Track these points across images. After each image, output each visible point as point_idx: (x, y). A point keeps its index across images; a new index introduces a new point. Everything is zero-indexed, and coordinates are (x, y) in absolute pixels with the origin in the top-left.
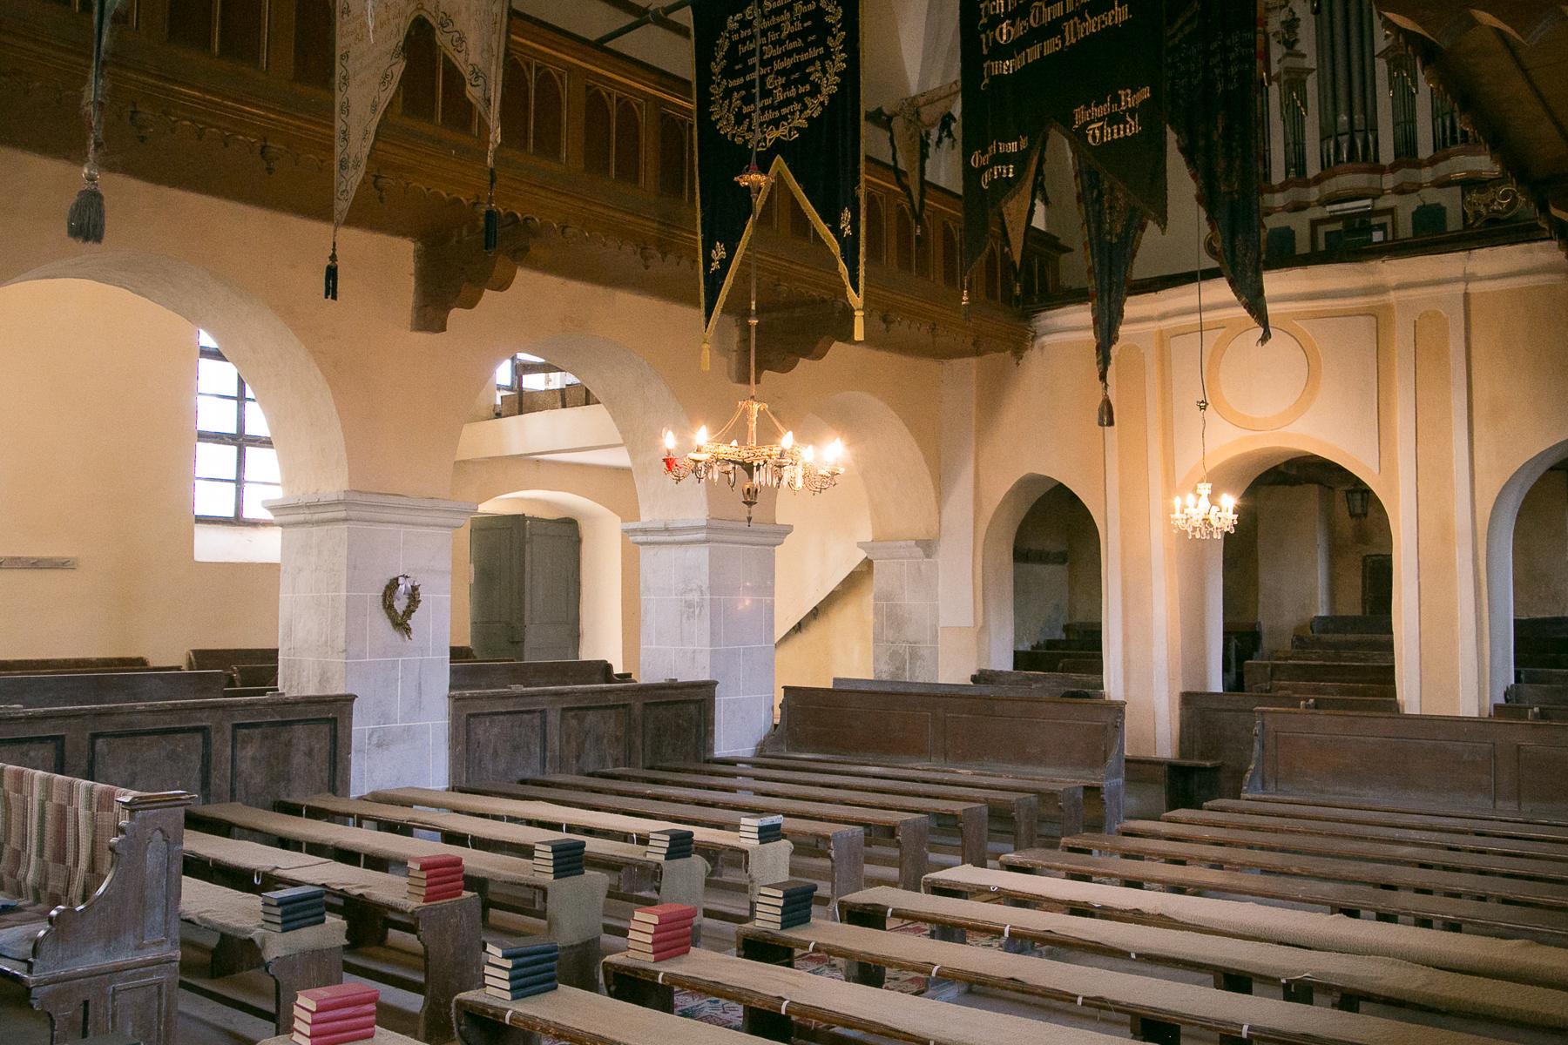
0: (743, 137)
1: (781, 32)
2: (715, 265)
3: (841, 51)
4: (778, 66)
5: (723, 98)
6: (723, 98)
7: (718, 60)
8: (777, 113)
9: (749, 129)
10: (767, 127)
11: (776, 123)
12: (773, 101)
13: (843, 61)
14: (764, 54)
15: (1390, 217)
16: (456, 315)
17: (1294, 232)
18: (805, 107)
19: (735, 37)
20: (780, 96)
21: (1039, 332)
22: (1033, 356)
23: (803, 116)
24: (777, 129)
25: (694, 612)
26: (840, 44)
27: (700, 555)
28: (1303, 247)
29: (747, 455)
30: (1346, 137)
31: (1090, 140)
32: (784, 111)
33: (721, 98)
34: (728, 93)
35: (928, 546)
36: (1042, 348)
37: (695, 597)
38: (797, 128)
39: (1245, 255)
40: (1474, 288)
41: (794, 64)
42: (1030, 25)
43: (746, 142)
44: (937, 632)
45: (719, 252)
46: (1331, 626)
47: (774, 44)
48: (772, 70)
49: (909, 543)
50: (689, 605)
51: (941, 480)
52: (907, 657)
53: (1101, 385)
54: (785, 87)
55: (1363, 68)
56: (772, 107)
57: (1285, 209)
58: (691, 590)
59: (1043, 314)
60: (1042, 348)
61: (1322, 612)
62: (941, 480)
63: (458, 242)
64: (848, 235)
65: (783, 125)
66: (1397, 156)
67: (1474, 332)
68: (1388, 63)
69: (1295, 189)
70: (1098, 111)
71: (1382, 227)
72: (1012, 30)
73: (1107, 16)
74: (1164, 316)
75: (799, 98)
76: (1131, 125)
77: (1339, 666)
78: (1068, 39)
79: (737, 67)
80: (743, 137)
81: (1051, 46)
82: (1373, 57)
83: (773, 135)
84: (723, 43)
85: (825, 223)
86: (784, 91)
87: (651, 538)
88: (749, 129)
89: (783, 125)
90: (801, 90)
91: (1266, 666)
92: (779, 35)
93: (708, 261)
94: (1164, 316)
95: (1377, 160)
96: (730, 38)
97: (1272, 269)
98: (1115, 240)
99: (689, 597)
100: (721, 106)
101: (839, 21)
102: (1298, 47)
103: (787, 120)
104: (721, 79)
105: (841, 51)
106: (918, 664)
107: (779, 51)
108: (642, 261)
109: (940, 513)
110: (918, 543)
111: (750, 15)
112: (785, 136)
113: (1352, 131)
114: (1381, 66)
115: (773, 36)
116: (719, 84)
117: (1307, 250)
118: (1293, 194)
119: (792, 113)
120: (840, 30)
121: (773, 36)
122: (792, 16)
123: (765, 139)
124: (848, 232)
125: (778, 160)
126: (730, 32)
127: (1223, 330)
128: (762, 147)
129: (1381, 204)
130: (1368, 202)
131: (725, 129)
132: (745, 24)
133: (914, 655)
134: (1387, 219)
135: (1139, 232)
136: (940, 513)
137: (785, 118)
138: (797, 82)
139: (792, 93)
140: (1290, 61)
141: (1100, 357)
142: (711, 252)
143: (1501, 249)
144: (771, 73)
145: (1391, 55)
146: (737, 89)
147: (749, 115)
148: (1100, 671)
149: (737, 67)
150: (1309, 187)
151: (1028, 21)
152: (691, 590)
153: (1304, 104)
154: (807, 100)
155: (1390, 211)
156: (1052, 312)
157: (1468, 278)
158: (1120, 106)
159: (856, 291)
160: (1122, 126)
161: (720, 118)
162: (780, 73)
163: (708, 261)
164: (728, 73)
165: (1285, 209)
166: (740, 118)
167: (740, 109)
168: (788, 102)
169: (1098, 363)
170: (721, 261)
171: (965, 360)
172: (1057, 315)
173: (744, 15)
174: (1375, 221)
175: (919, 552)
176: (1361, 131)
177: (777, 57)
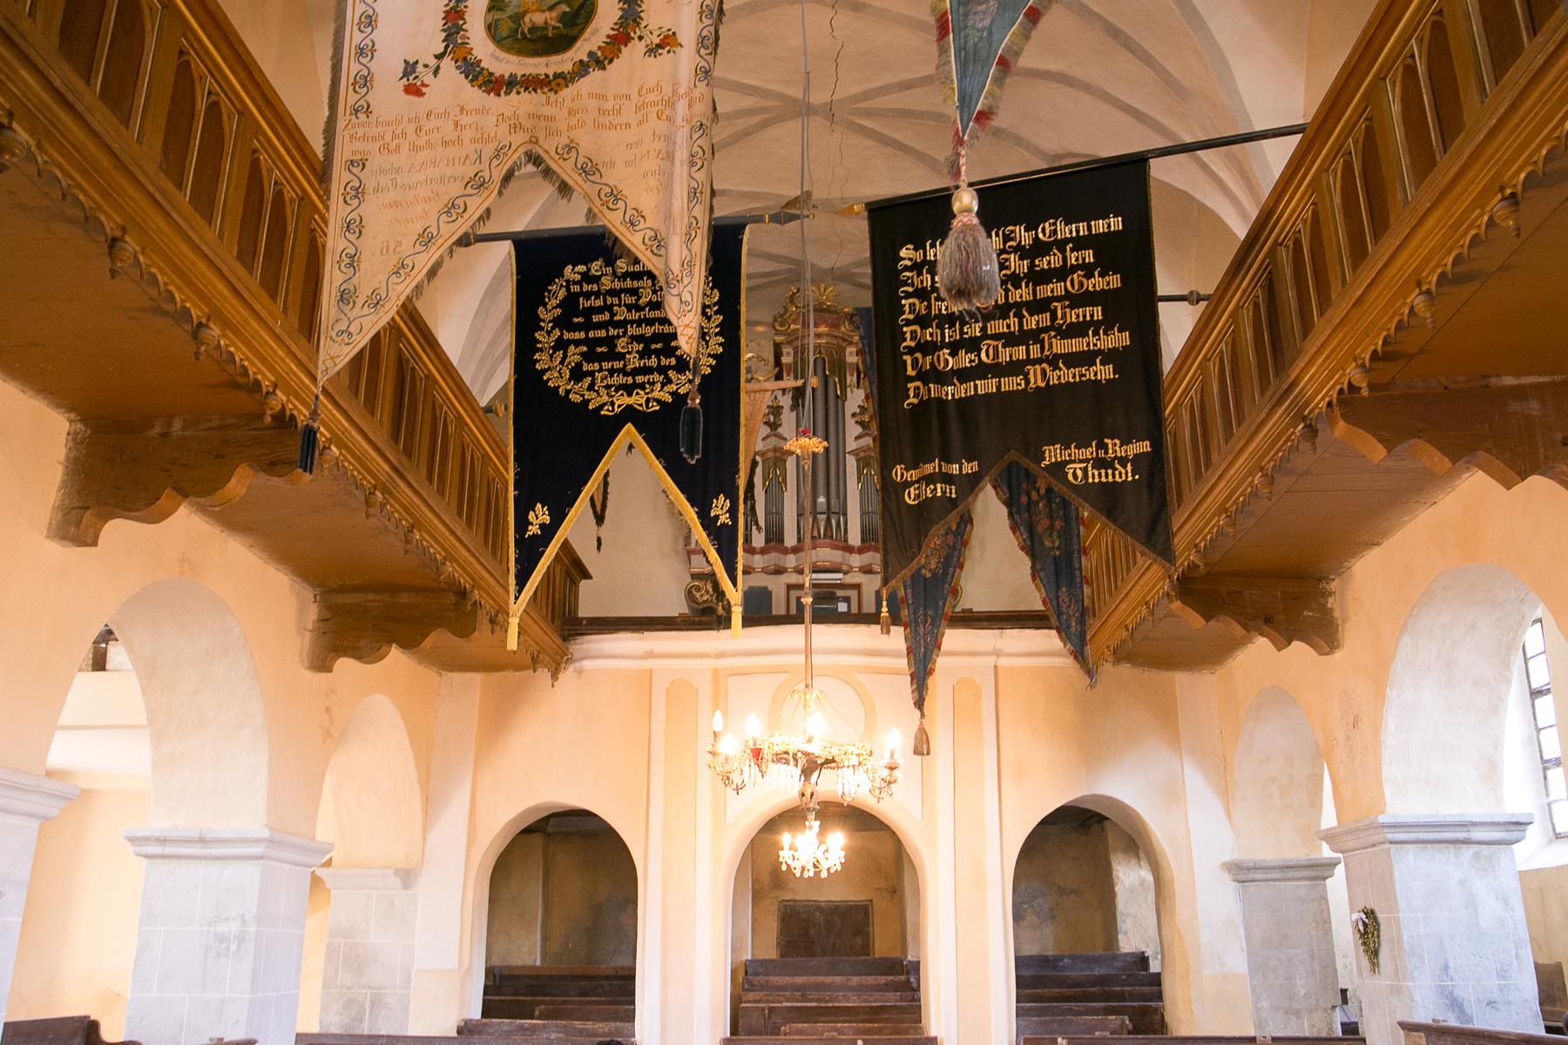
0: (583, 396)
1: (639, 298)
2: (534, 530)
3: (716, 335)
4: (632, 330)
5: (555, 349)
6: (555, 349)
7: (549, 307)
8: (630, 380)
9: (591, 388)
10: (616, 391)
11: (629, 390)
12: (625, 366)
13: (720, 345)
14: (616, 315)
15: (856, 592)
16: (117, 531)
17: (771, 592)
18: (669, 381)
19: (576, 288)
20: (634, 362)
21: (576, 655)
22: (567, 675)
23: (666, 389)
24: (630, 395)
25: (228, 948)
26: (717, 327)
27: (250, 875)
28: (778, 608)
29: (838, 752)
30: (824, 516)
31: (1070, 477)
32: (640, 379)
33: (553, 347)
34: (561, 345)
35: (407, 876)
36: (580, 672)
37: (233, 928)
38: (658, 401)
39: (1069, 607)
40: (1003, 662)
41: (654, 334)
42: (980, 359)
43: (586, 402)
44: (410, 976)
45: (540, 516)
46: (761, 970)
47: (629, 308)
48: (625, 333)
49: (386, 871)
50: (222, 938)
51: (431, 801)
52: (367, 1006)
53: (918, 713)
54: (642, 355)
55: (838, 458)
56: (623, 371)
57: (765, 571)
58: (227, 919)
59: (585, 637)
60: (580, 672)
61: (749, 958)
62: (431, 801)
63: (163, 435)
64: (724, 525)
65: (637, 394)
66: (863, 540)
67: (1001, 699)
68: (857, 460)
69: (777, 554)
70: (1088, 453)
71: (847, 600)
72: (950, 359)
73: (1088, 370)
74: (721, 655)
75: (662, 370)
76: (1120, 473)
77: (834, 1007)
78: (1032, 380)
79: (576, 320)
80: (583, 396)
81: (1011, 384)
82: (845, 453)
83: (623, 400)
84: (558, 292)
85: (692, 506)
86: (640, 359)
87: (169, 850)
88: (591, 388)
89: (637, 394)
90: (664, 362)
91: (763, 1009)
92: (637, 300)
93: (521, 523)
94: (721, 655)
95: (846, 540)
96: (568, 289)
97: (840, 623)
98: (928, 575)
99: (222, 928)
100: (551, 356)
101: (715, 304)
102: (780, 430)
103: (643, 389)
104: (553, 328)
105: (716, 335)
106: (383, 1013)
107: (635, 316)
108: (364, 507)
109: (424, 839)
110: (397, 872)
111: (596, 271)
112: (641, 405)
113: (829, 512)
114: (851, 462)
115: (631, 300)
116: (549, 333)
117: (783, 612)
118: (773, 558)
119: (653, 384)
120: (716, 313)
121: (631, 300)
122: (654, 285)
123: (613, 404)
124: (724, 519)
125: (629, 428)
126: (568, 281)
127: (786, 675)
128: (608, 410)
129: (849, 579)
130: (840, 576)
131: (558, 379)
132: (587, 278)
133: (376, 1003)
134: (853, 594)
135: (958, 570)
136: (424, 839)
137: (642, 386)
138: (658, 353)
139: (653, 362)
140: (773, 441)
141: (915, 686)
142: (528, 514)
143: (1027, 631)
144: (624, 336)
145: (862, 455)
146: (577, 343)
147: (591, 374)
148: (630, 1017)
149: (576, 320)
150: (786, 554)
151: (979, 355)
152: (227, 919)
153: (785, 480)
154: (671, 374)
155: (857, 587)
156: (594, 637)
157: (998, 653)
158: (1106, 453)
159: (735, 585)
160: (1110, 471)
161: (549, 369)
162: (634, 338)
163: (521, 523)
164: (562, 322)
165: (765, 571)
166: (577, 374)
167: (579, 365)
168: (647, 370)
169: (913, 692)
170: (542, 526)
171: (468, 675)
172: (588, 642)
173: (589, 269)
174: (840, 593)
175: (398, 882)
176: (821, 513)
177: (632, 322)
